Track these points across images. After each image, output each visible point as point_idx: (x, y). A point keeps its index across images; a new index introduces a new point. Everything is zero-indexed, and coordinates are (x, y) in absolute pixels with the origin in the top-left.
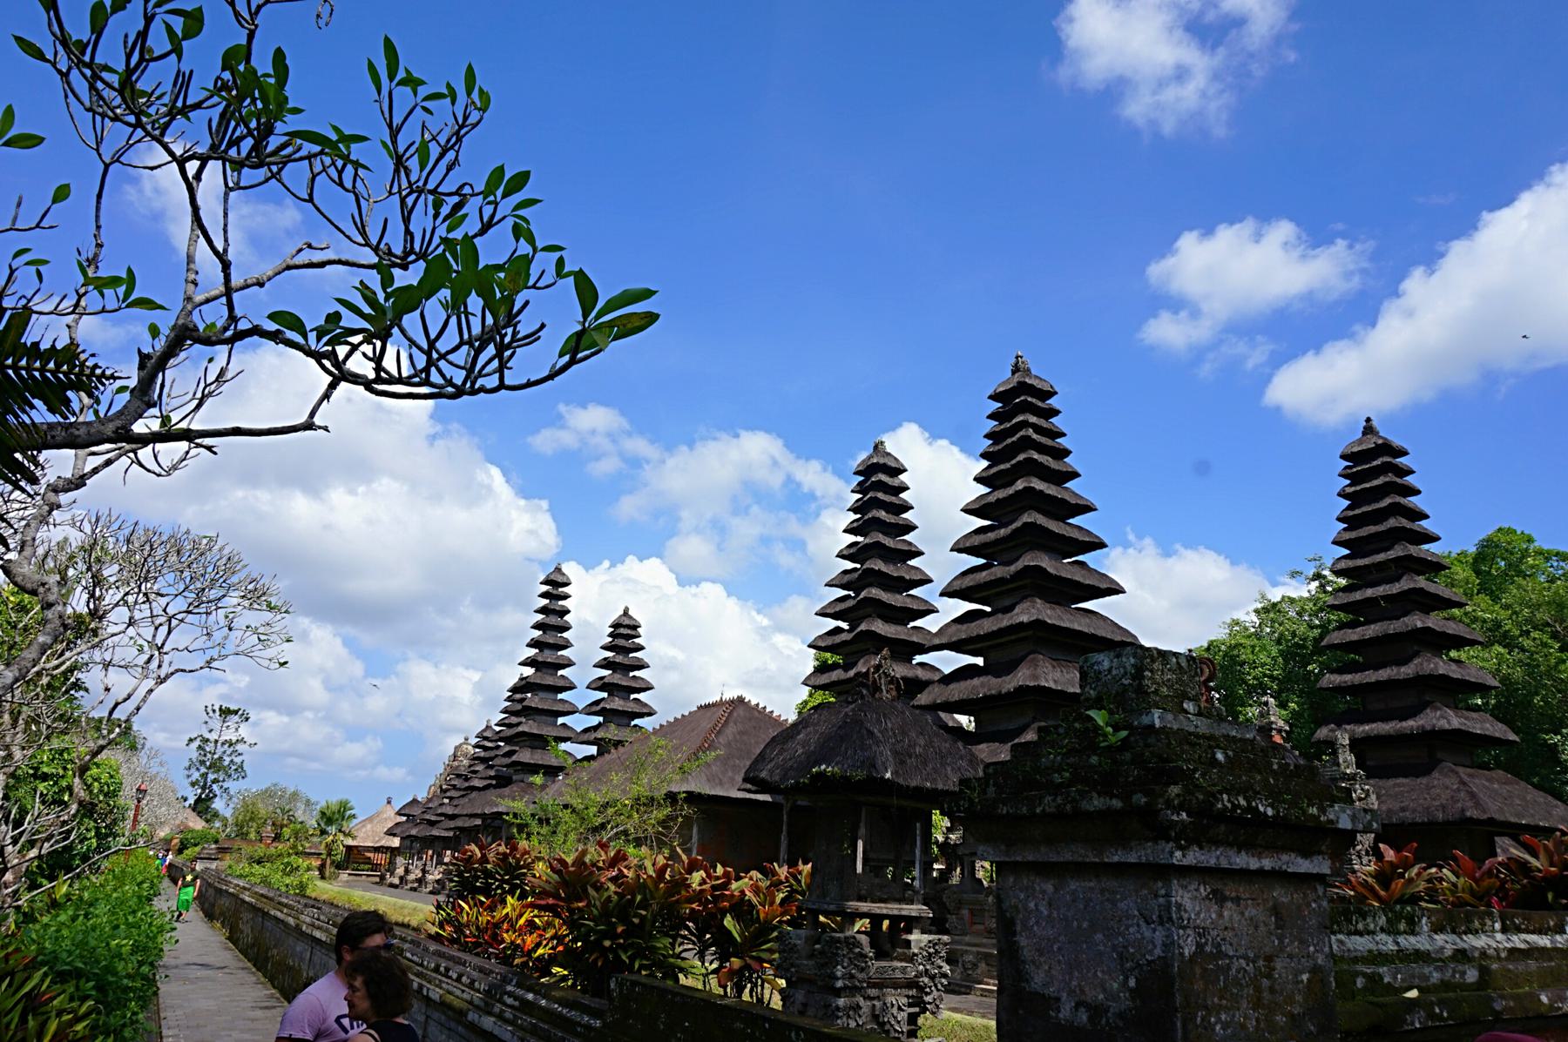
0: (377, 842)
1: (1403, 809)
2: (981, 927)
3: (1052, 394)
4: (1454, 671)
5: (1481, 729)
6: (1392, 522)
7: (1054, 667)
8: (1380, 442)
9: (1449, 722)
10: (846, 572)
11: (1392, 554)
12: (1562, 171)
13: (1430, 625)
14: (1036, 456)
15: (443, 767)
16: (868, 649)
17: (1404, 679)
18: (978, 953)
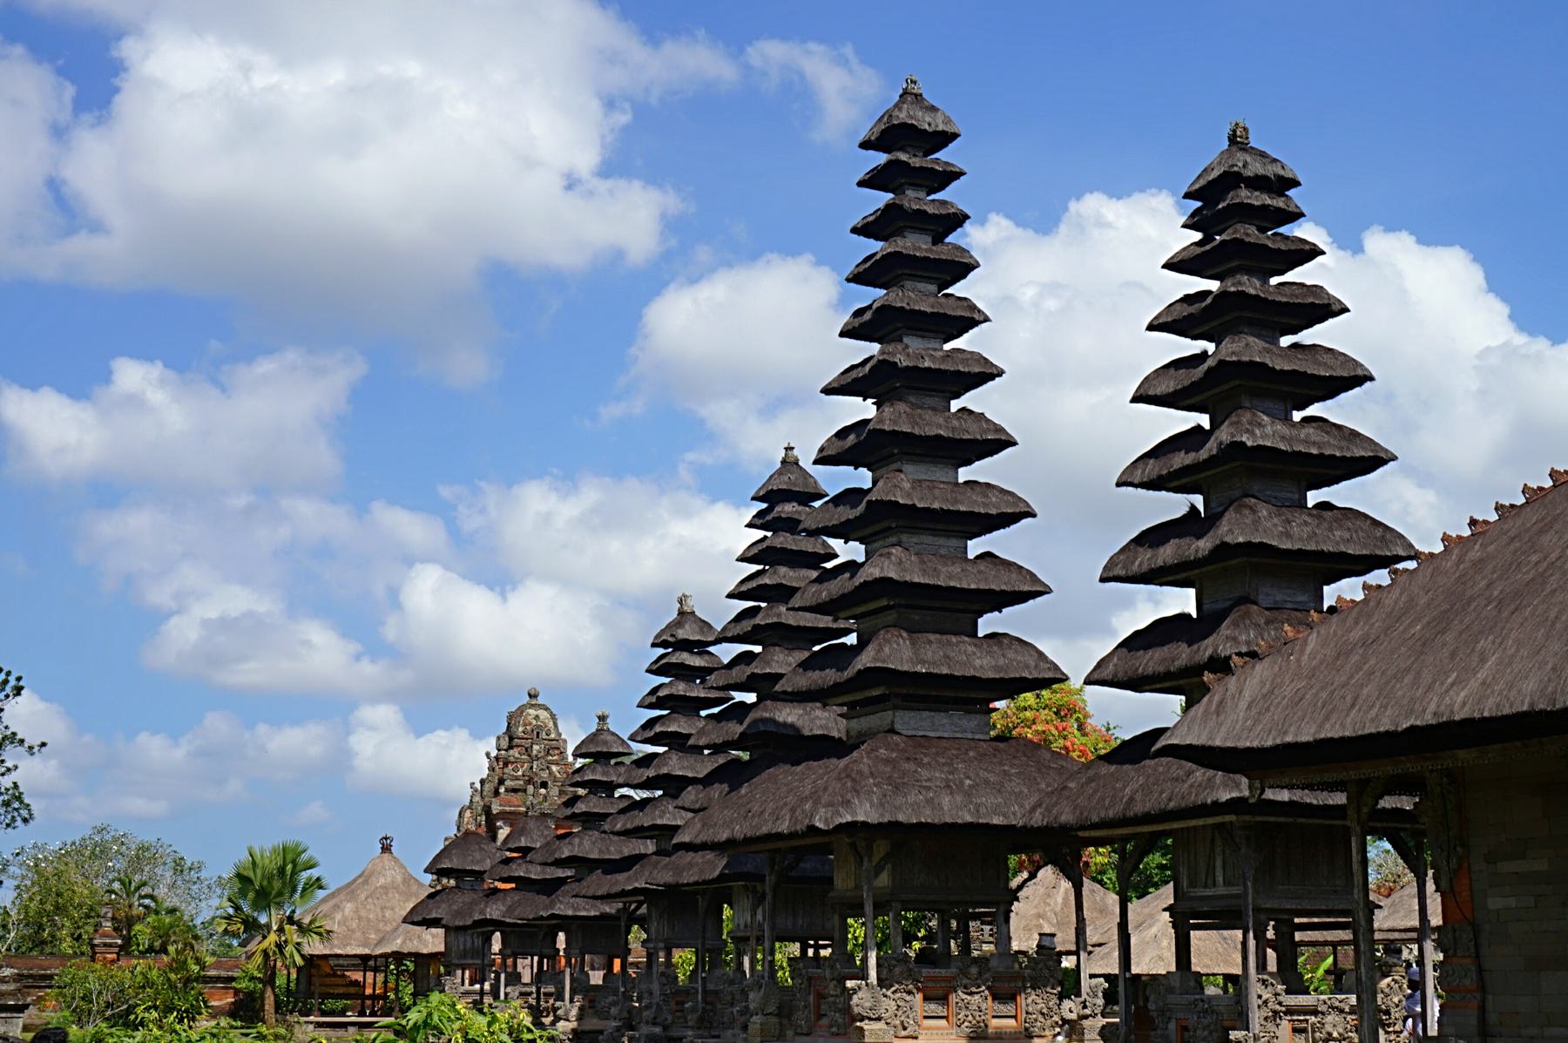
0: (379, 943)
15: (486, 763)
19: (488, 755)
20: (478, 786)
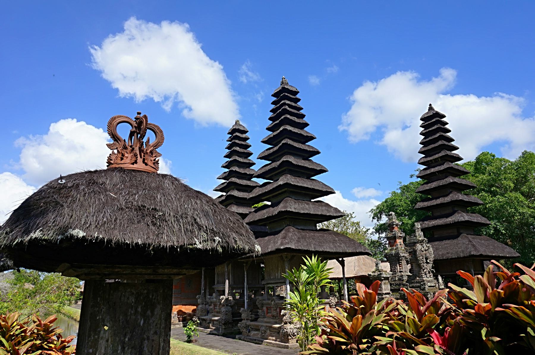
1: (448, 253)
2: (270, 314)
4: (465, 198)
5: (477, 220)
6: (440, 143)
7: (295, 203)
8: (435, 112)
9: (464, 218)
10: (225, 173)
11: (440, 155)
12: (506, 143)
13: (456, 181)
14: (288, 116)
16: (233, 203)
17: (447, 203)
18: (267, 326)
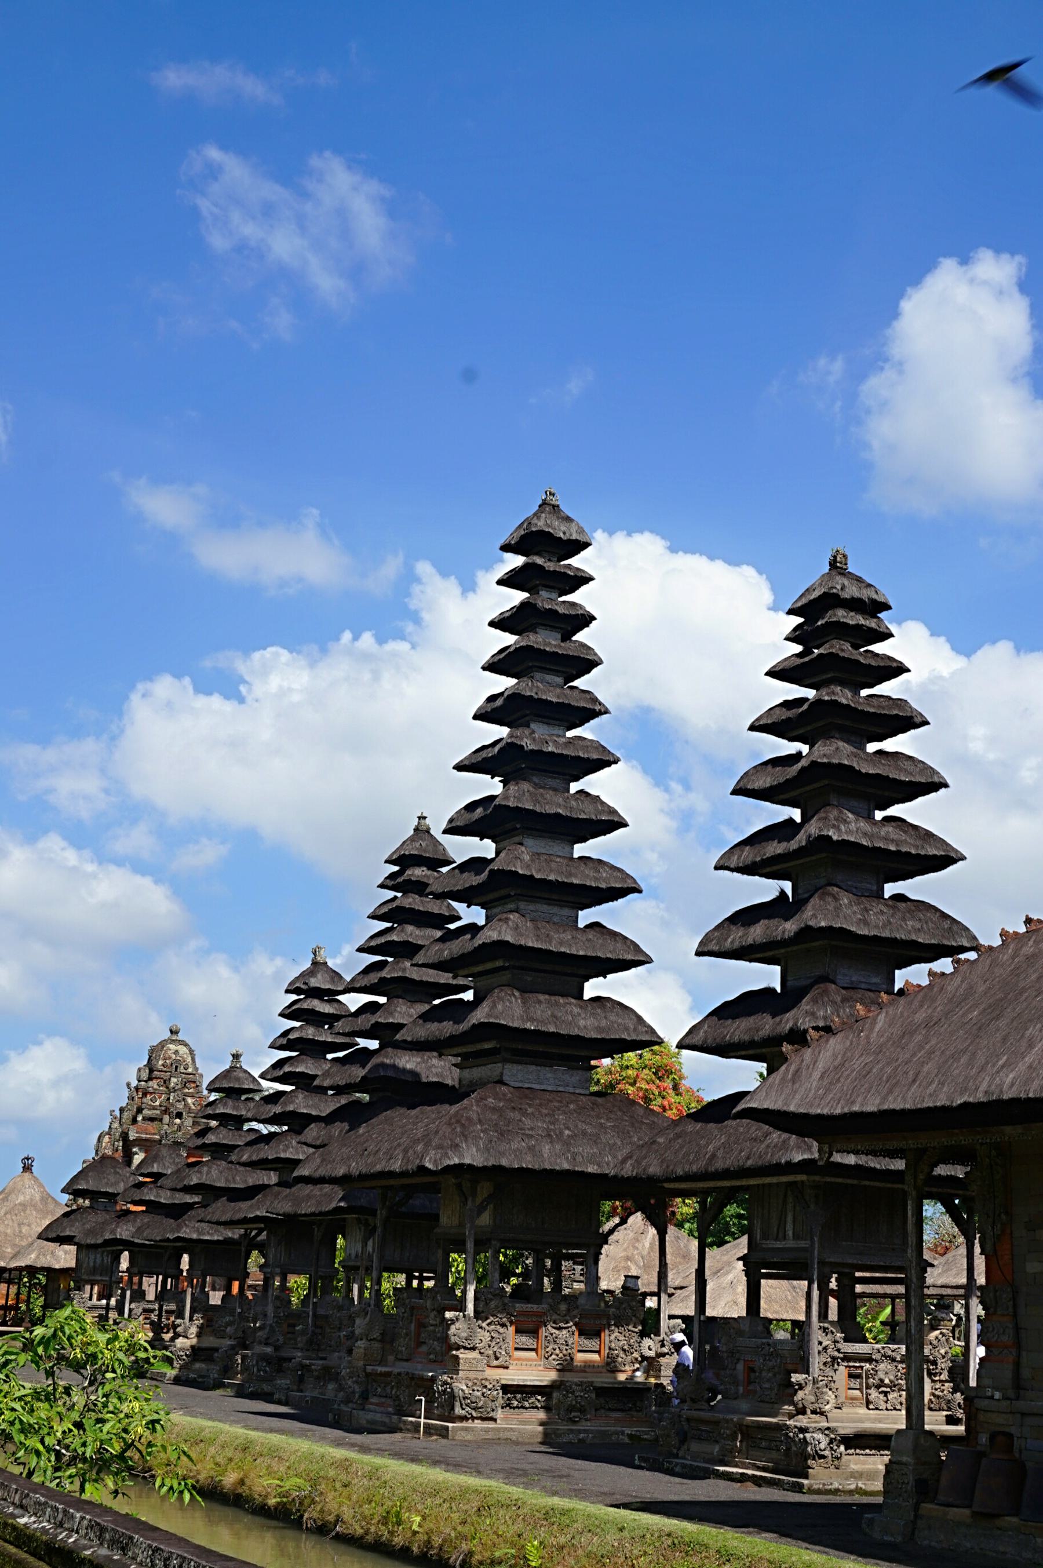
0: (14, 1256)
3: (578, 546)
15: (126, 1093)
19: (128, 1085)
20: (117, 1113)
